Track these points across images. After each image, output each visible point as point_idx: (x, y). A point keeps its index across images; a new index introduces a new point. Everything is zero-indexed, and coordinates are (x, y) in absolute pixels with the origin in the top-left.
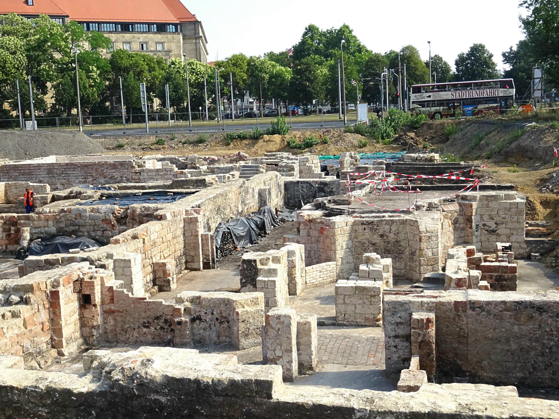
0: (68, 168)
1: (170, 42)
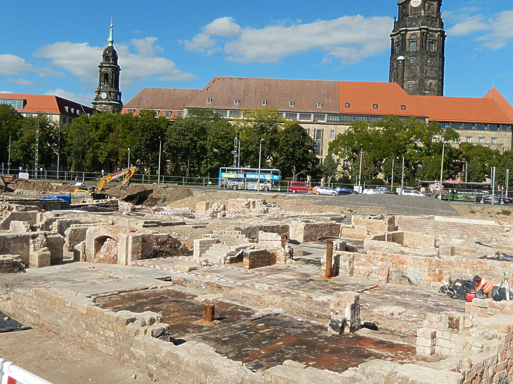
0: (450, 226)
1: (503, 138)
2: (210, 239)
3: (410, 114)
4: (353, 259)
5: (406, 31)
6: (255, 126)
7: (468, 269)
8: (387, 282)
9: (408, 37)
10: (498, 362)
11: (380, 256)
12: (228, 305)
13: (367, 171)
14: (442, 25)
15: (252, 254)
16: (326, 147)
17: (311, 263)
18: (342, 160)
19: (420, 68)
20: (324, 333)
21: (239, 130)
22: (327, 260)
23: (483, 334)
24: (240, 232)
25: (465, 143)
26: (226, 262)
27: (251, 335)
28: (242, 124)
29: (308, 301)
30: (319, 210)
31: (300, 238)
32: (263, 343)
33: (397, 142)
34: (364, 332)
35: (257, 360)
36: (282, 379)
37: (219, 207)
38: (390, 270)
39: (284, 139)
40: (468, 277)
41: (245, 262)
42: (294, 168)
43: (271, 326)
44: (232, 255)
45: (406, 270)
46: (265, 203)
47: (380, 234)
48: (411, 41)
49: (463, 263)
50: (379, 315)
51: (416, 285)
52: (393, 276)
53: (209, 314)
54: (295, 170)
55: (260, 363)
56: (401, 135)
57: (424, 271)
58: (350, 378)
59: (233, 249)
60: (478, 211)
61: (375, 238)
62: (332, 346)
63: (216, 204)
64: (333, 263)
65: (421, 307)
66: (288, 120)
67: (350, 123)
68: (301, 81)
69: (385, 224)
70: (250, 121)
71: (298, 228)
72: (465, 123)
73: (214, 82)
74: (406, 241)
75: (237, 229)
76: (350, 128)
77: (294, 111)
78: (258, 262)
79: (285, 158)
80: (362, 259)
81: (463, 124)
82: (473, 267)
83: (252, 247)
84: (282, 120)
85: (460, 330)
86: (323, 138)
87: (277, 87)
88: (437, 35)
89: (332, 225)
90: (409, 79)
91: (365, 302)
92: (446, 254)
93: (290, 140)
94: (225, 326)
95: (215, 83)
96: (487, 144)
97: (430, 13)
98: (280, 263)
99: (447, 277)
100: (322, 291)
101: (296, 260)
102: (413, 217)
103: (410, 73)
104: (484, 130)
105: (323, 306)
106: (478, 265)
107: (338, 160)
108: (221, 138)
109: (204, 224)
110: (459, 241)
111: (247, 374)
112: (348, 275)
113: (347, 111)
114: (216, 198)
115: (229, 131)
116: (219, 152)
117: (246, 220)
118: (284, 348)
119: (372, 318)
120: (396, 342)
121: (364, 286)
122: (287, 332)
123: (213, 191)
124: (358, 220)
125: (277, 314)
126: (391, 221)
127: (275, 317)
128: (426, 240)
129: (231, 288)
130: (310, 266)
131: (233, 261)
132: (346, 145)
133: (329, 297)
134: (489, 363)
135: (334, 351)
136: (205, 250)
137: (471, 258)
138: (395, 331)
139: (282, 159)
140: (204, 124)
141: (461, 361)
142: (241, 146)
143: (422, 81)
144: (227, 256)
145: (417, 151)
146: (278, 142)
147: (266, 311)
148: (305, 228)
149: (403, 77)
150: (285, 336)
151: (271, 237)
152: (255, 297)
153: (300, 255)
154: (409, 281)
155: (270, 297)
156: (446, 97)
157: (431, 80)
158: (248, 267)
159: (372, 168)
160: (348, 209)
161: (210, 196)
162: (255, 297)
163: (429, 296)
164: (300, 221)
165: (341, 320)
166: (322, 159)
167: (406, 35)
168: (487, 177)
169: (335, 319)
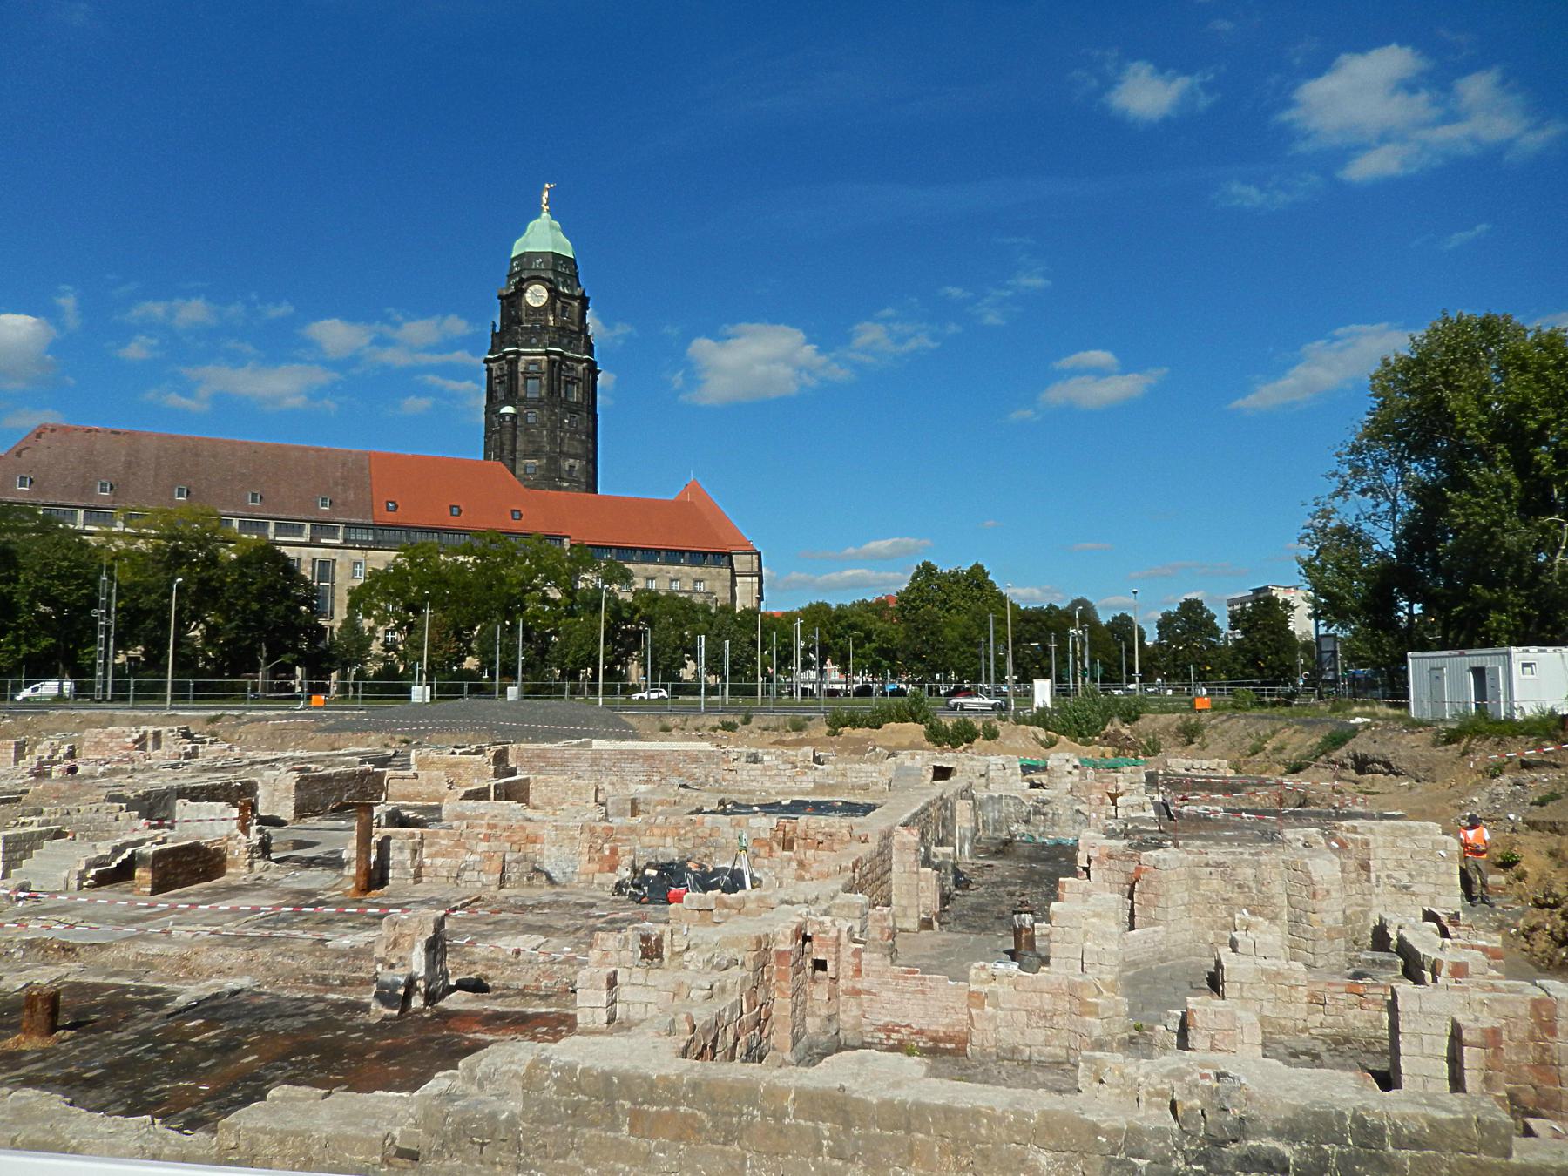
2: (34, 828)
3: (530, 528)
4: (421, 844)
5: (519, 354)
6: (157, 548)
8: (500, 888)
9: (521, 367)
10: (742, 1014)
11: (484, 830)
12: (96, 989)
13: (441, 652)
14: (590, 349)
15: (159, 856)
16: (342, 601)
17: (318, 865)
18: (381, 629)
19: (549, 435)
20: (361, 1018)
21: (113, 559)
22: (359, 850)
23: (709, 961)
24: (124, 805)
25: (643, 591)
26: (85, 884)
27: (166, 1054)
28: (120, 543)
29: (315, 951)
30: (329, 745)
31: (286, 811)
32: (202, 1065)
33: (505, 588)
34: (457, 1001)
35: (189, 1109)
36: (266, 1134)
37: (55, 752)
38: (507, 858)
39: (234, 581)
40: (669, 855)
41: (140, 877)
42: (264, 649)
43: (222, 1021)
44: (102, 865)
45: (541, 854)
46: (187, 735)
47: (478, 785)
48: (528, 375)
49: (658, 827)
50: (488, 960)
51: (565, 886)
52: (514, 873)
53: (41, 1017)
54: (265, 655)
55: (198, 1114)
56: (512, 573)
57: (581, 853)
58: (440, 1095)
59: (104, 849)
60: (676, 726)
61: (469, 796)
62: (384, 1042)
63: (47, 743)
64: (373, 857)
65: (578, 929)
66: (245, 536)
67: (398, 547)
68: (279, 447)
69: (488, 763)
70: (143, 536)
71: (281, 786)
72: (643, 550)
73: (39, 436)
74: (534, 797)
75: (113, 799)
76: (399, 556)
77: (262, 514)
78: (177, 875)
79: (238, 627)
80: (442, 842)
81: (639, 552)
82: (678, 834)
83: (159, 839)
84: (231, 536)
85: (666, 961)
86: (333, 578)
87: (214, 456)
88: (580, 368)
89: (367, 773)
90: (526, 455)
91: (454, 934)
92: (621, 814)
93: (252, 584)
94: (90, 1041)
95: (42, 441)
96: (685, 592)
97: (567, 322)
98: (237, 872)
99: (627, 860)
100: (350, 924)
101: (277, 861)
102: (547, 745)
103: (529, 442)
104: (678, 564)
105: (355, 958)
106: (688, 828)
107: (372, 630)
108: (58, 577)
109: (15, 793)
110: (643, 788)
111: (168, 1143)
112: (411, 881)
113: (390, 518)
114: (46, 730)
115: (83, 559)
116: (54, 613)
117: (139, 776)
118: (260, 1067)
119: (473, 967)
120: (530, 1010)
121: (448, 902)
122: (267, 1029)
123: (36, 714)
124: (426, 758)
125: (238, 992)
126: (500, 758)
127: (231, 1000)
128: (578, 792)
129: (102, 947)
130: (315, 872)
131: (103, 880)
132: (390, 594)
133: (369, 935)
134: (726, 1018)
135: (388, 1055)
136: (21, 860)
137: (673, 814)
138: (525, 987)
139: (231, 629)
140: (8, 542)
141: (673, 1021)
142: (120, 597)
143: (554, 460)
144: (89, 867)
145: (547, 608)
146: (220, 588)
147: (206, 989)
148: (298, 786)
149: (513, 451)
150: (261, 1041)
151: (210, 811)
152: (172, 961)
153: (286, 850)
154: (549, 878)
155: (215, 955)
156: (604, 497)
157: (571, 461)
158: (149, 889)
159: (453, 645)
160: (398, 737)
161: (27, 726)
162: (172, 961)
163: (592, 905)
164: (284, 770)
165: (402, 980)
166: (332, 628)
167: (517, 362)
168: (689, 659)
169: (388, 979)
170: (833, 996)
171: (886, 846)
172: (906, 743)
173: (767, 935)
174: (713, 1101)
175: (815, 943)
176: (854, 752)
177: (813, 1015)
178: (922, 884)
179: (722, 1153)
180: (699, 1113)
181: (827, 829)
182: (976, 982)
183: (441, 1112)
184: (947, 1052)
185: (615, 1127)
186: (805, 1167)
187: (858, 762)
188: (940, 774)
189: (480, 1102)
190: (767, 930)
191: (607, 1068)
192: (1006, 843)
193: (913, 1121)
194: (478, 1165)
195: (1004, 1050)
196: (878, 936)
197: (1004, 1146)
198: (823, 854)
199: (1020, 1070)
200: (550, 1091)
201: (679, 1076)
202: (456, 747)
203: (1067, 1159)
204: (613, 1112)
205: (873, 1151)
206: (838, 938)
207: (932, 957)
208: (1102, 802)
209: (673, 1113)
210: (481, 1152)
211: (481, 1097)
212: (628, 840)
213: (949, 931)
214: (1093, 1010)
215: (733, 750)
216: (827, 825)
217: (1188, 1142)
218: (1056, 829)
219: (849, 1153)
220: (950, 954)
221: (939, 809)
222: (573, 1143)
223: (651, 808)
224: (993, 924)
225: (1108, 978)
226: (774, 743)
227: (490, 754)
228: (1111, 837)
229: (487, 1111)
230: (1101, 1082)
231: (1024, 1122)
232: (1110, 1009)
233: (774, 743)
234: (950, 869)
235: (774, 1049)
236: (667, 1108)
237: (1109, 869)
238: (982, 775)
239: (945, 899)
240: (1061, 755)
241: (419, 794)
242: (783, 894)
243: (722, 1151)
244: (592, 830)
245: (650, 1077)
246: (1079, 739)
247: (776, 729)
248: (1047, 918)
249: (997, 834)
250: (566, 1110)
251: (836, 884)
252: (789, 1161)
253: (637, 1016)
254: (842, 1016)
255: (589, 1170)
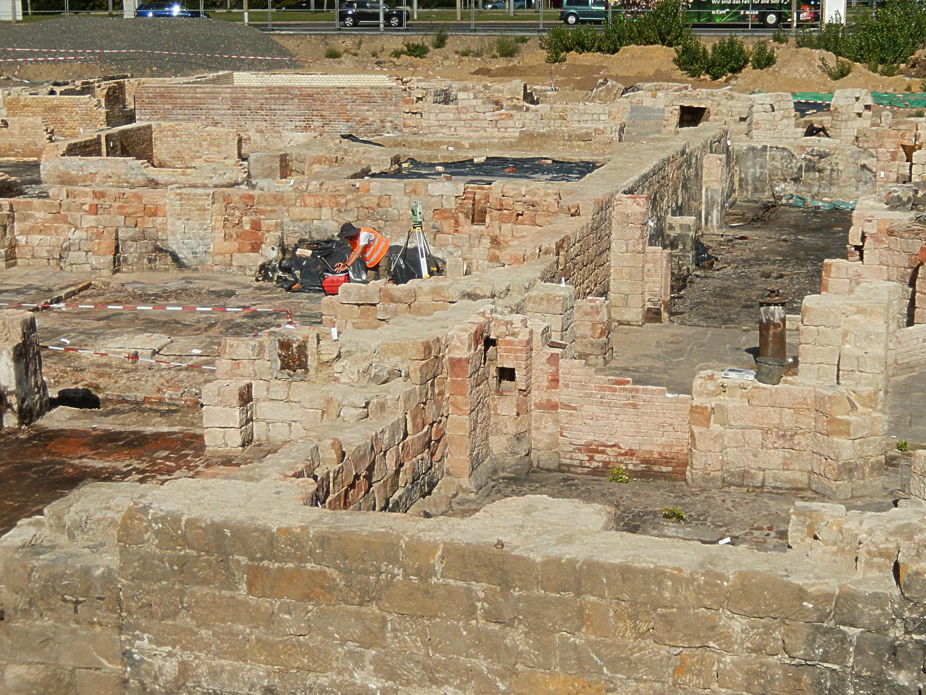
0: (274, 98)
7: (324, 210)
10: (406, 435)
38: (121, 235)
40: (326, 230)
45: (164, 230)
47: (85, 134)
49: (311, 195)
50: (99, 366)
51: (196, 270)
52: (131, 252)
57: (214, 228)
58: (23, 546)
60: (346, 51)
61: (73, 150)
65: (211, 326)
74: (160, 150)
80: (37, 215)
82: (337, 204)
85: (312, 372)
92: (268, 174)
99: (271, 238)
106: (350, 197)
119: (80, 375)
120: (149, 430)
121: (50, 290)
124: (17, 100)
126: (115, 97)
128: (215, 143)
134: (386, 442)
137: (330, 178)
138: (146, 400)
154: (176, 259)
170: (522, 410)
171: (603, 220)
172: (651, 72)
173: (438, 340)
174: (346, 558)
175: (501, 348)
176: (581, 86)
177: (498, 432)
178: (649, 266)
179: (358, 616)
180: (328, 571)
181: (528, 197)
182: (700, 394)
183: (25, 567)
184: (662, 475)
185: (230, 584)
186: (456, 631)
187: (586, 99)
188: (686, 117)
189: (71, 555)
190: (438, 333)
191: (217, 519)
192: (767, 207)
193: (583, 583)
194: (74, 626)
195: (732, 475)
196: (589, 333)
197: (692, 611)
198: (525, 229)
199: (749, 498)
200: (151, 545)
201: (304, 529)
202: (56, 84)
203: (764, 626)
204: (227, 569)
205: (535, 615)
206: (529, 342)
207: (658, 357)
208: (894, 156)
209: (298, 570)
210: (76, 611)
211: (73, 549)
212: (273, 211)
213: (682, 323)
214: (843, 429)
215: (417, 84)
216: (528, 192)
217: (910, 609)
218: (834, 189)
219: (508, 615)
220: (679, 352)
221: (679, 168)
222: (182, 603)
223: (306, 167)
224: (738, 314)
225: (866, 390)
226: (476, 73)
227: (101, 90)
228: (893, 208)
229: (78, 566)
230: (816, 538)
231: (716, 585)
232: (864, 428)
233: (476, 73)
234: (689, 244)
235: (449, 474)
236: (291, 565)
237: (889, 249)
238: (743, 119)
239: (680, 282)
240: (849, 91)
241: (11, 147)
242: (467, 284)
243: (357, 612)
244: (227, 200)
245: (269, 530)
246: (880, 67)
247: (478, 55)
248: (796, 311)
249: (757, 196)
250: (171, 565)
251: (532, 271)
252: (436, 625)
253: (280, 437)
254: (534, 433)
255: (203, 632)
